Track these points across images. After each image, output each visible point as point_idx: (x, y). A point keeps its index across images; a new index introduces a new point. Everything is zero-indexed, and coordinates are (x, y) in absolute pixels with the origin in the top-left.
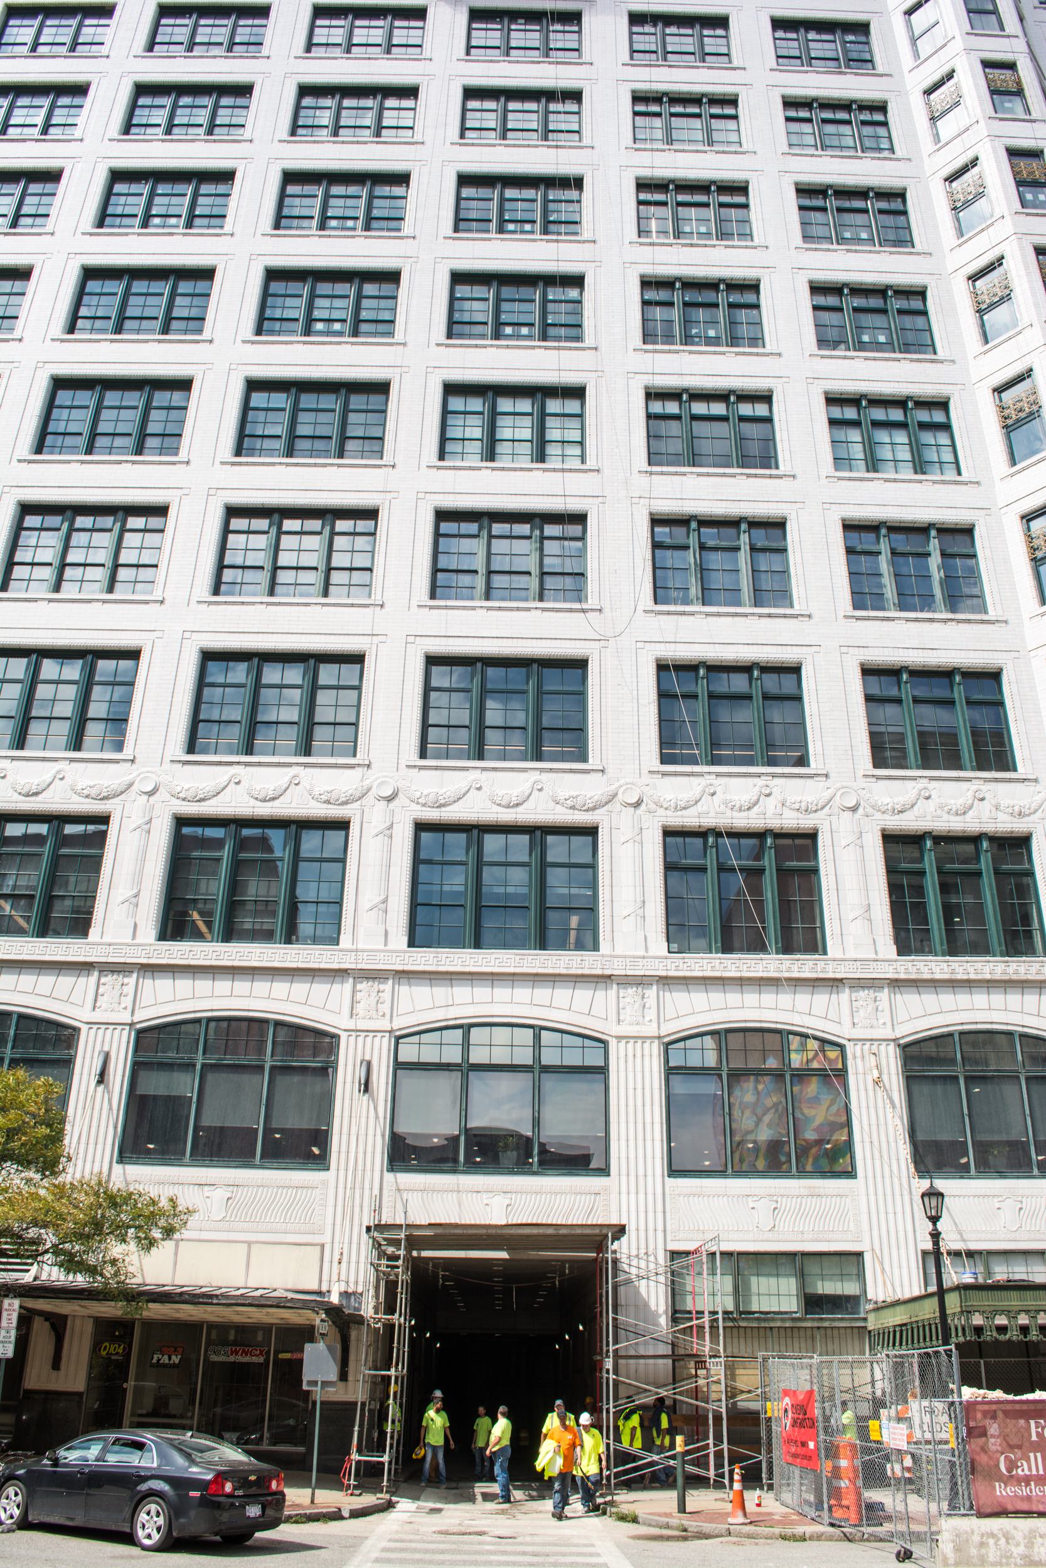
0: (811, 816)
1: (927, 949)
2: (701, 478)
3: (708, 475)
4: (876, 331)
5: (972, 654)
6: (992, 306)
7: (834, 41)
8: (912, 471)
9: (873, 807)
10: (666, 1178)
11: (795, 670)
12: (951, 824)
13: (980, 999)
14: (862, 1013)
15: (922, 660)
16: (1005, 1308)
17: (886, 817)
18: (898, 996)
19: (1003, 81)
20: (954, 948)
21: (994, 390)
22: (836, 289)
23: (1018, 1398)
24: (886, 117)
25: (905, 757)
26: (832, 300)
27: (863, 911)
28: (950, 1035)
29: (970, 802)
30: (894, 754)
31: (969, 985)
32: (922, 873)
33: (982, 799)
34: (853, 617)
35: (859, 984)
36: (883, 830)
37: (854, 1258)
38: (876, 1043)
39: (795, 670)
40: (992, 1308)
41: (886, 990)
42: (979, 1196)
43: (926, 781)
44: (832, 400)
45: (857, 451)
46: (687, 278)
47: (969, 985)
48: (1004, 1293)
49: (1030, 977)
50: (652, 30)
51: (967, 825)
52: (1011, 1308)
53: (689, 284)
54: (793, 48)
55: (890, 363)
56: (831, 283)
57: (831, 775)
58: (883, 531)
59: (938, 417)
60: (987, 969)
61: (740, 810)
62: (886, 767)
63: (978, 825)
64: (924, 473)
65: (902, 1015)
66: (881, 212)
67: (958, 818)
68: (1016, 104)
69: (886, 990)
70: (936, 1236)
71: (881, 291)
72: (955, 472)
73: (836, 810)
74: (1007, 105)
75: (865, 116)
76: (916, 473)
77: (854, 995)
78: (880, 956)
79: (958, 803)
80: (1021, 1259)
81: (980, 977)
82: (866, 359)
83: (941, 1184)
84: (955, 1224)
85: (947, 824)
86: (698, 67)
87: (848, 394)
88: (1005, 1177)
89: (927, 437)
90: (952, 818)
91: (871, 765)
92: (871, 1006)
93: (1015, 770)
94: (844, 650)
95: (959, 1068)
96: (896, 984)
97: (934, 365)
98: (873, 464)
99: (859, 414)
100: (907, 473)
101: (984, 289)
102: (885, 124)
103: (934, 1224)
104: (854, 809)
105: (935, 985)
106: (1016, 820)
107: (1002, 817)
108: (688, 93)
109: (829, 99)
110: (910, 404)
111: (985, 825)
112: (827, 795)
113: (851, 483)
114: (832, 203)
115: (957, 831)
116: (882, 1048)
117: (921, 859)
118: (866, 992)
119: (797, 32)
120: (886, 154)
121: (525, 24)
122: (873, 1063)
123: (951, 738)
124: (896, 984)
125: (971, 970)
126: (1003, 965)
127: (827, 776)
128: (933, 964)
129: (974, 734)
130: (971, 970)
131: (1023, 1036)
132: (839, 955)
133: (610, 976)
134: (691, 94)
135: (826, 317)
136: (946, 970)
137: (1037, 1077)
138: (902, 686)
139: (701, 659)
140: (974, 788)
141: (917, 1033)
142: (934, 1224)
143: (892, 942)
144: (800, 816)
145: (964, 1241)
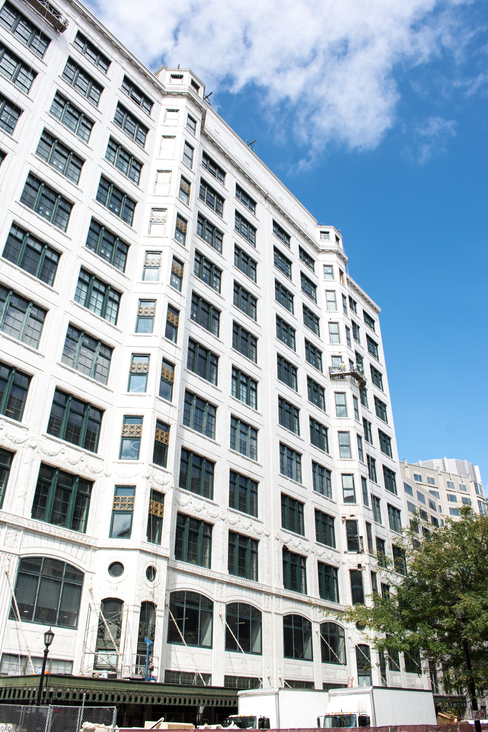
0: (16, 445)
1: (42, 518)
2: (21, 274)
3: (25, 274)
4: (107, 251)
5: (97, 400)
6: (150, 267)
7: (88, 85)
8: (100, 314)
9: (41, 450)
10: (8, 619)
11: (29, 377)
12: (69, 468)
13: (56, 545)
14: (9, 540)
15: (79, 394)
16: (63, 686)
17: (45, 456)
18: (26, 536)
19: (185, 187)
20: (53, 521)
21: (140, 299)
22: (40, 181)
23: (131, 728)
24: (92, 128)
25: (59, 432)
26: (35, 185)
27: (23, 494)
28: (41, 558)
29: (78, 461)
30: (55, 429)
31: (54, 538)
32: (50, 484)
33: (83, 461)
34: (60, 365)
35: (12, 526)
36: (42, 461)
37: (69, 663)
38: (11, 555)
39: (29, 377)
40: (58, 686)
41: (22, 532)
42: (32, 631)
43: (65, 446)
44: (15, 225)
45: (83, 296)
46: (48, 184)
47: (54, 538)
48: (64, 680)
49: (78, 541)
50: (74, 70)
51: (74, 470)
52: (65, 686)
53: (48, 187)
54: (71, 74)
55: (108, 267)
56: (99, 222)
57: (29, 429)
58: (11, 293)
59: (116, 298)
60: (63, 533)
61: (72, 464)
62: (50, 434)
63: (78, 471)
64: (88, 308)
65: (25, 545)
66: (56, 150)
67: (72, 466)
68: (184, 197)
69: (22, 532)
70: (46, 652)
71: (115, 237)
72: (114, 323)
73: (26, 446)
74: (183, 197)
75: (134, 164)
76: (85, 306)
77: (8, 530)
78: (24, 516)
79: (74, 459)
80: (63, 663)
81: (60, 536)
82: (101, 261)
83: (54, 630)
84: (19, 642)
85: (67, 467)
86: (9, 33)
87: (89, 271)
88: (44, 625)
89: (110, 304)
90: (70, 465)
91: (46, 431)
92: (14, 537)
93: (96, 452)
94: (52, 377)
95: (40, 574)
96: (27, 530)
97: (123, 277)
98: (87, 304)
99: (23, 238)
100: (98, 314)
101: (150, 259)
102: (90, 130)
103: (47, 647)
104: (34, 448)
105: (41, 534)
106: (91, 474)
107: (87, 471)
108: (78, 107)
109: (125, 148)
110: (28, 235)
111: (80, 472)
112: (26, 438)
113: (78, 308)
114: (55, 146)
115: (69, 471)
116: (13, 557)
117: (51, 478)
118: (14, 530)
119: (89, 82)
120: (135, 183)
121: (26, 25)
122: (7, 564)
123: (78, 430)
124: (27, 530)
125: (57, 532)
126: (70, 533)
127: (28, 429)
128: (44, 525)
129: (68, 424)
130: (57, 532)
131: (68, 565)
132: (8, 512)
133: (90, 546)
134: (79, 108)
135: (30, 190)
136: (48, 530)
137: (68, 583)
138: (11, 375)
139: (72, 393)
140: (81, 455)
141: (28, 554)
142: (47, 647)
143: (31, 511)
144: (12, 443)
145: (21, 650)
